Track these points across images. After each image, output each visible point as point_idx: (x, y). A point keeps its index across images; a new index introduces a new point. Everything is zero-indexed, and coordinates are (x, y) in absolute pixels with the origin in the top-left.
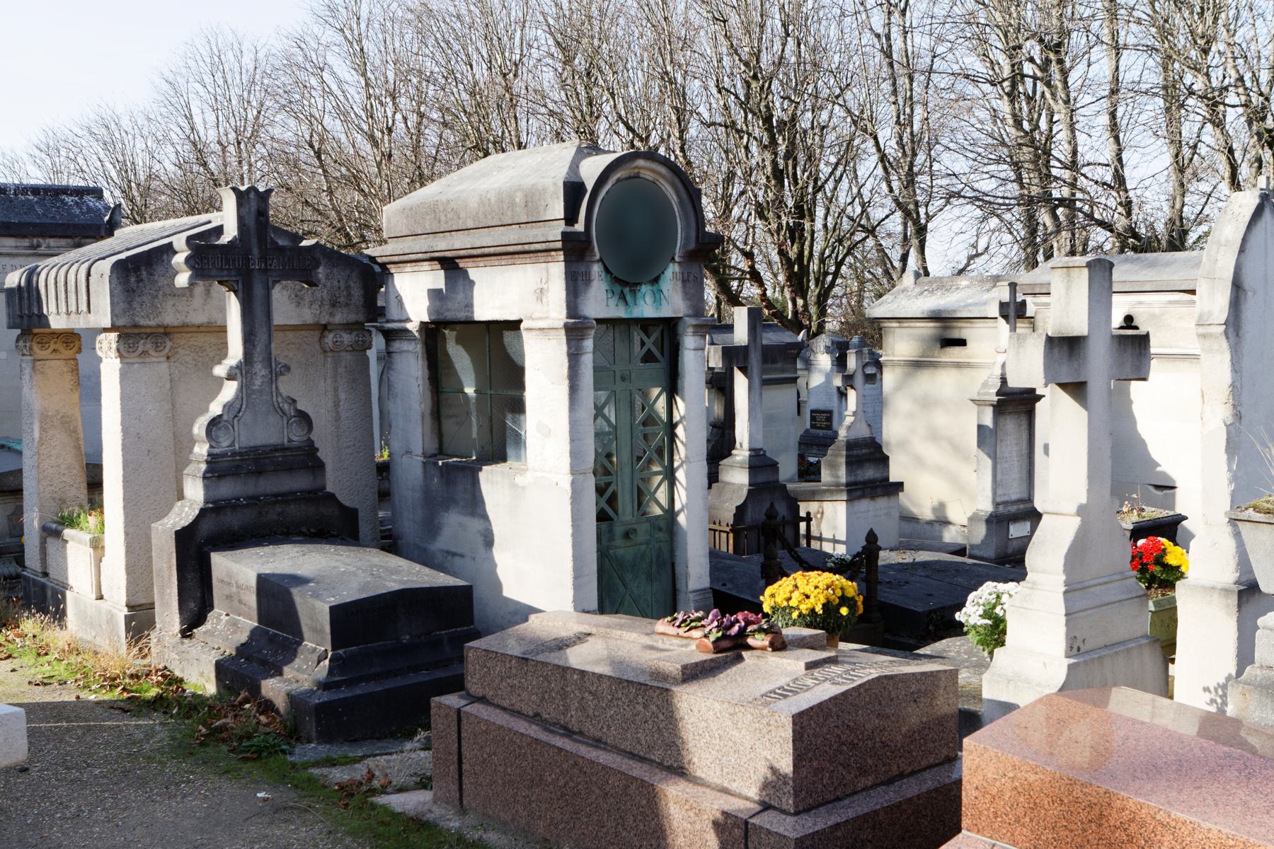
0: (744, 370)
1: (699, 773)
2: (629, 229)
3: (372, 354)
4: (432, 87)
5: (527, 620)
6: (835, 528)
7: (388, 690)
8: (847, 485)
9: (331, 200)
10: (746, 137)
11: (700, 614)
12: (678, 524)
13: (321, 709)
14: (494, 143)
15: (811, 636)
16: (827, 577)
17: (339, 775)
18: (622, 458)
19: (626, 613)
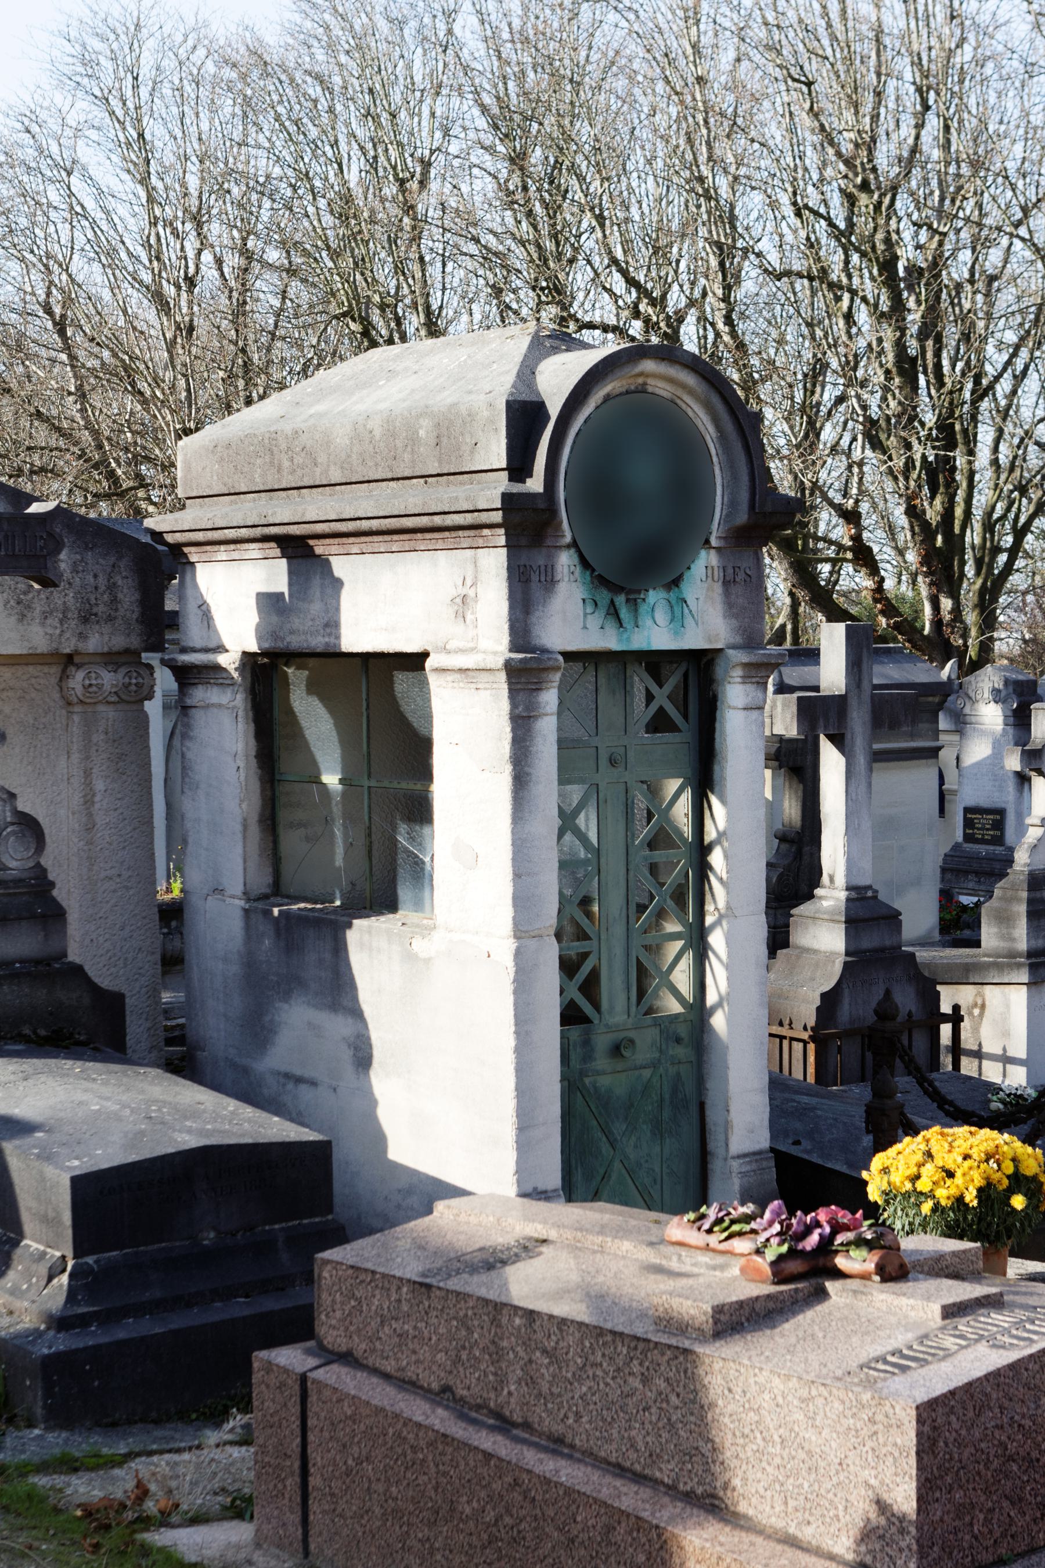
0: (838, 741)
1: (743, 1507)
2: (624, 486)
3: (153, 708)
4: (267, 204)
5: (430, 1211)
6: (1006, 1034)
7: (175, 1333)
8: (1030, 954)
9: (83, 410)
10: (846, 297)
11: (749, 1209)
12: (711, 1030)
13: (55, 1367)
14: (383, 307)
15: (954, 1254)
16: (986, 1138)
17: (83, 1489)
18: (611, 906)
19: (610, 1200)
